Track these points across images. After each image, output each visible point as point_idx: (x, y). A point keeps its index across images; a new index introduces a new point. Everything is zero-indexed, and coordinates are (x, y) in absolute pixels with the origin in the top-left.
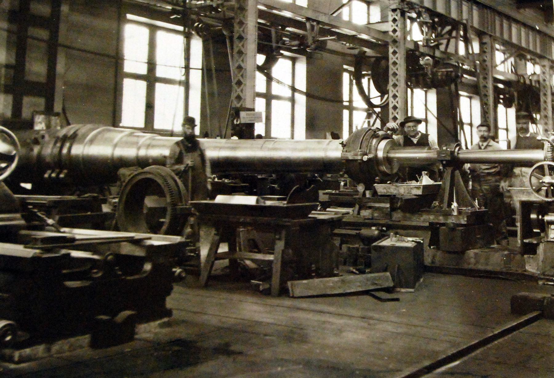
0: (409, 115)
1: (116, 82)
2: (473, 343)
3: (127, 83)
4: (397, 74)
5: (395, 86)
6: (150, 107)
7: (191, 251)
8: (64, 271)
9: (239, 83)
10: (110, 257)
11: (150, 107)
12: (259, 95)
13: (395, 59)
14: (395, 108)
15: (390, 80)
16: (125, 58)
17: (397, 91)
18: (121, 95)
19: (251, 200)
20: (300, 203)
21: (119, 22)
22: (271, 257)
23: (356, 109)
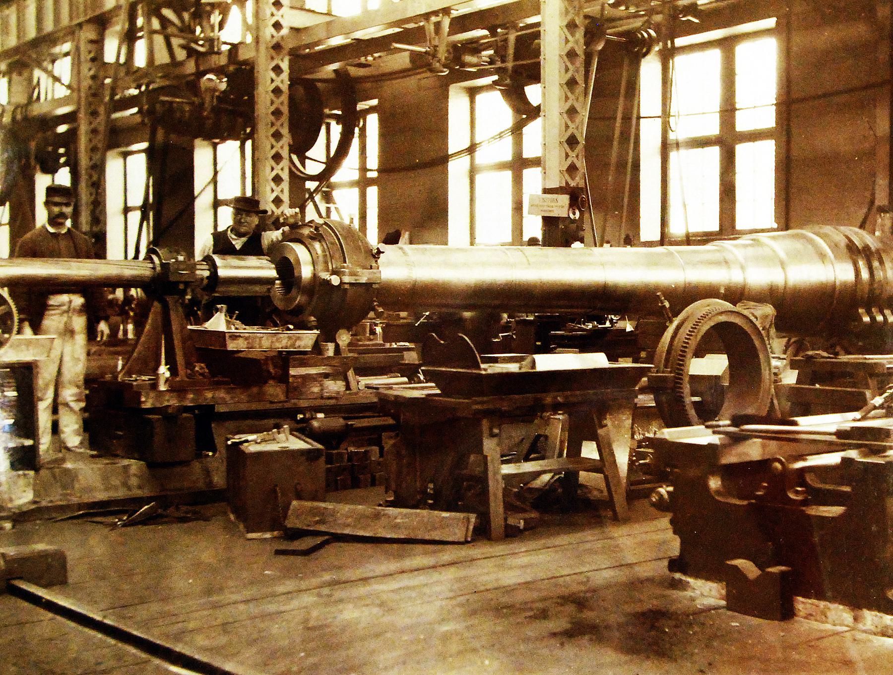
0: (249, 144)
1: (788, 120)
2: (135, 633)
3: (768, 119)
4: (273, 135)
5: (277, 91)
6: (728, 192)
7: (643, 456)
8: (847, 489)
9: (572, 141)
10: (778, 465)
11: (728, 192)
12: (536, 162)
13: (277, 102)
14: (277, 180)
15: (286, 102)
16: (774, 108)
17: (272, 81)
18: (777, 196)
19: (546, 362)
20: (454, 368)
21: (783, 268)
22: (508, 469)
23: (353, 184)
